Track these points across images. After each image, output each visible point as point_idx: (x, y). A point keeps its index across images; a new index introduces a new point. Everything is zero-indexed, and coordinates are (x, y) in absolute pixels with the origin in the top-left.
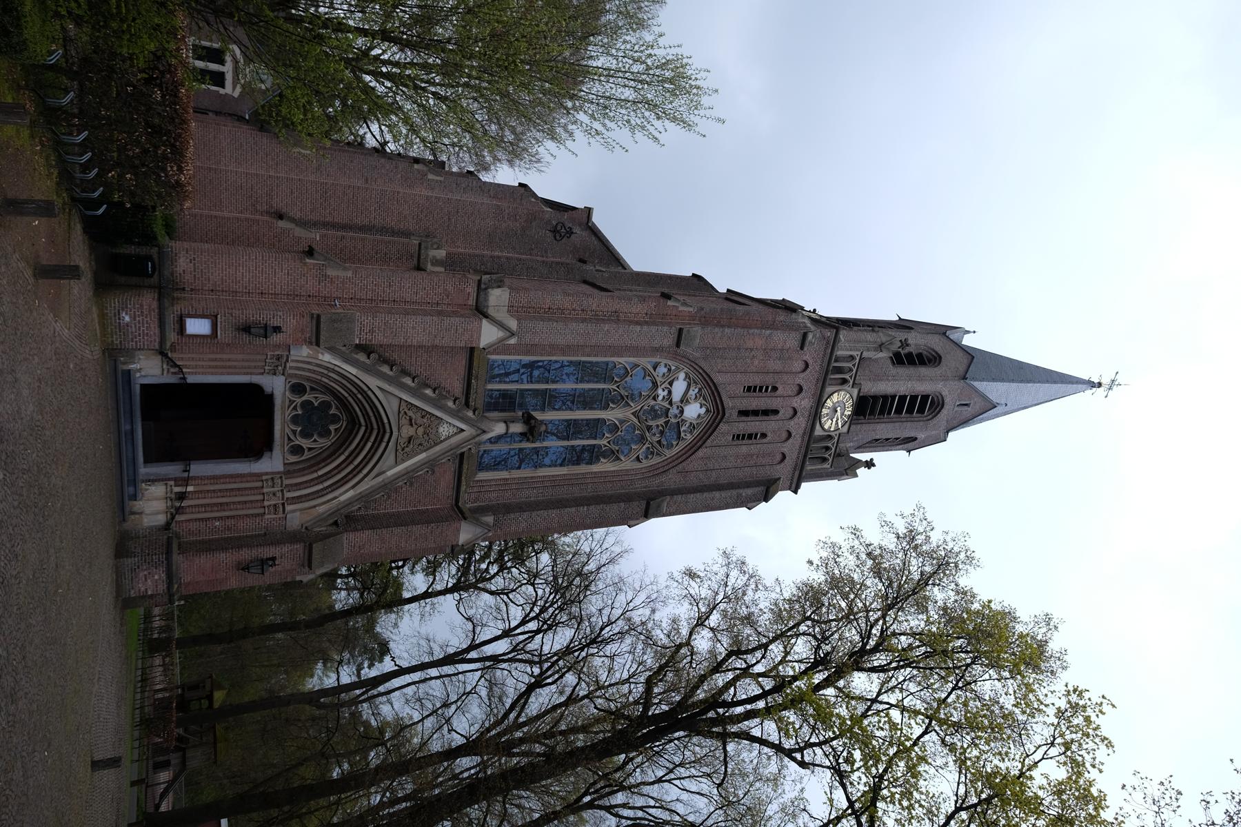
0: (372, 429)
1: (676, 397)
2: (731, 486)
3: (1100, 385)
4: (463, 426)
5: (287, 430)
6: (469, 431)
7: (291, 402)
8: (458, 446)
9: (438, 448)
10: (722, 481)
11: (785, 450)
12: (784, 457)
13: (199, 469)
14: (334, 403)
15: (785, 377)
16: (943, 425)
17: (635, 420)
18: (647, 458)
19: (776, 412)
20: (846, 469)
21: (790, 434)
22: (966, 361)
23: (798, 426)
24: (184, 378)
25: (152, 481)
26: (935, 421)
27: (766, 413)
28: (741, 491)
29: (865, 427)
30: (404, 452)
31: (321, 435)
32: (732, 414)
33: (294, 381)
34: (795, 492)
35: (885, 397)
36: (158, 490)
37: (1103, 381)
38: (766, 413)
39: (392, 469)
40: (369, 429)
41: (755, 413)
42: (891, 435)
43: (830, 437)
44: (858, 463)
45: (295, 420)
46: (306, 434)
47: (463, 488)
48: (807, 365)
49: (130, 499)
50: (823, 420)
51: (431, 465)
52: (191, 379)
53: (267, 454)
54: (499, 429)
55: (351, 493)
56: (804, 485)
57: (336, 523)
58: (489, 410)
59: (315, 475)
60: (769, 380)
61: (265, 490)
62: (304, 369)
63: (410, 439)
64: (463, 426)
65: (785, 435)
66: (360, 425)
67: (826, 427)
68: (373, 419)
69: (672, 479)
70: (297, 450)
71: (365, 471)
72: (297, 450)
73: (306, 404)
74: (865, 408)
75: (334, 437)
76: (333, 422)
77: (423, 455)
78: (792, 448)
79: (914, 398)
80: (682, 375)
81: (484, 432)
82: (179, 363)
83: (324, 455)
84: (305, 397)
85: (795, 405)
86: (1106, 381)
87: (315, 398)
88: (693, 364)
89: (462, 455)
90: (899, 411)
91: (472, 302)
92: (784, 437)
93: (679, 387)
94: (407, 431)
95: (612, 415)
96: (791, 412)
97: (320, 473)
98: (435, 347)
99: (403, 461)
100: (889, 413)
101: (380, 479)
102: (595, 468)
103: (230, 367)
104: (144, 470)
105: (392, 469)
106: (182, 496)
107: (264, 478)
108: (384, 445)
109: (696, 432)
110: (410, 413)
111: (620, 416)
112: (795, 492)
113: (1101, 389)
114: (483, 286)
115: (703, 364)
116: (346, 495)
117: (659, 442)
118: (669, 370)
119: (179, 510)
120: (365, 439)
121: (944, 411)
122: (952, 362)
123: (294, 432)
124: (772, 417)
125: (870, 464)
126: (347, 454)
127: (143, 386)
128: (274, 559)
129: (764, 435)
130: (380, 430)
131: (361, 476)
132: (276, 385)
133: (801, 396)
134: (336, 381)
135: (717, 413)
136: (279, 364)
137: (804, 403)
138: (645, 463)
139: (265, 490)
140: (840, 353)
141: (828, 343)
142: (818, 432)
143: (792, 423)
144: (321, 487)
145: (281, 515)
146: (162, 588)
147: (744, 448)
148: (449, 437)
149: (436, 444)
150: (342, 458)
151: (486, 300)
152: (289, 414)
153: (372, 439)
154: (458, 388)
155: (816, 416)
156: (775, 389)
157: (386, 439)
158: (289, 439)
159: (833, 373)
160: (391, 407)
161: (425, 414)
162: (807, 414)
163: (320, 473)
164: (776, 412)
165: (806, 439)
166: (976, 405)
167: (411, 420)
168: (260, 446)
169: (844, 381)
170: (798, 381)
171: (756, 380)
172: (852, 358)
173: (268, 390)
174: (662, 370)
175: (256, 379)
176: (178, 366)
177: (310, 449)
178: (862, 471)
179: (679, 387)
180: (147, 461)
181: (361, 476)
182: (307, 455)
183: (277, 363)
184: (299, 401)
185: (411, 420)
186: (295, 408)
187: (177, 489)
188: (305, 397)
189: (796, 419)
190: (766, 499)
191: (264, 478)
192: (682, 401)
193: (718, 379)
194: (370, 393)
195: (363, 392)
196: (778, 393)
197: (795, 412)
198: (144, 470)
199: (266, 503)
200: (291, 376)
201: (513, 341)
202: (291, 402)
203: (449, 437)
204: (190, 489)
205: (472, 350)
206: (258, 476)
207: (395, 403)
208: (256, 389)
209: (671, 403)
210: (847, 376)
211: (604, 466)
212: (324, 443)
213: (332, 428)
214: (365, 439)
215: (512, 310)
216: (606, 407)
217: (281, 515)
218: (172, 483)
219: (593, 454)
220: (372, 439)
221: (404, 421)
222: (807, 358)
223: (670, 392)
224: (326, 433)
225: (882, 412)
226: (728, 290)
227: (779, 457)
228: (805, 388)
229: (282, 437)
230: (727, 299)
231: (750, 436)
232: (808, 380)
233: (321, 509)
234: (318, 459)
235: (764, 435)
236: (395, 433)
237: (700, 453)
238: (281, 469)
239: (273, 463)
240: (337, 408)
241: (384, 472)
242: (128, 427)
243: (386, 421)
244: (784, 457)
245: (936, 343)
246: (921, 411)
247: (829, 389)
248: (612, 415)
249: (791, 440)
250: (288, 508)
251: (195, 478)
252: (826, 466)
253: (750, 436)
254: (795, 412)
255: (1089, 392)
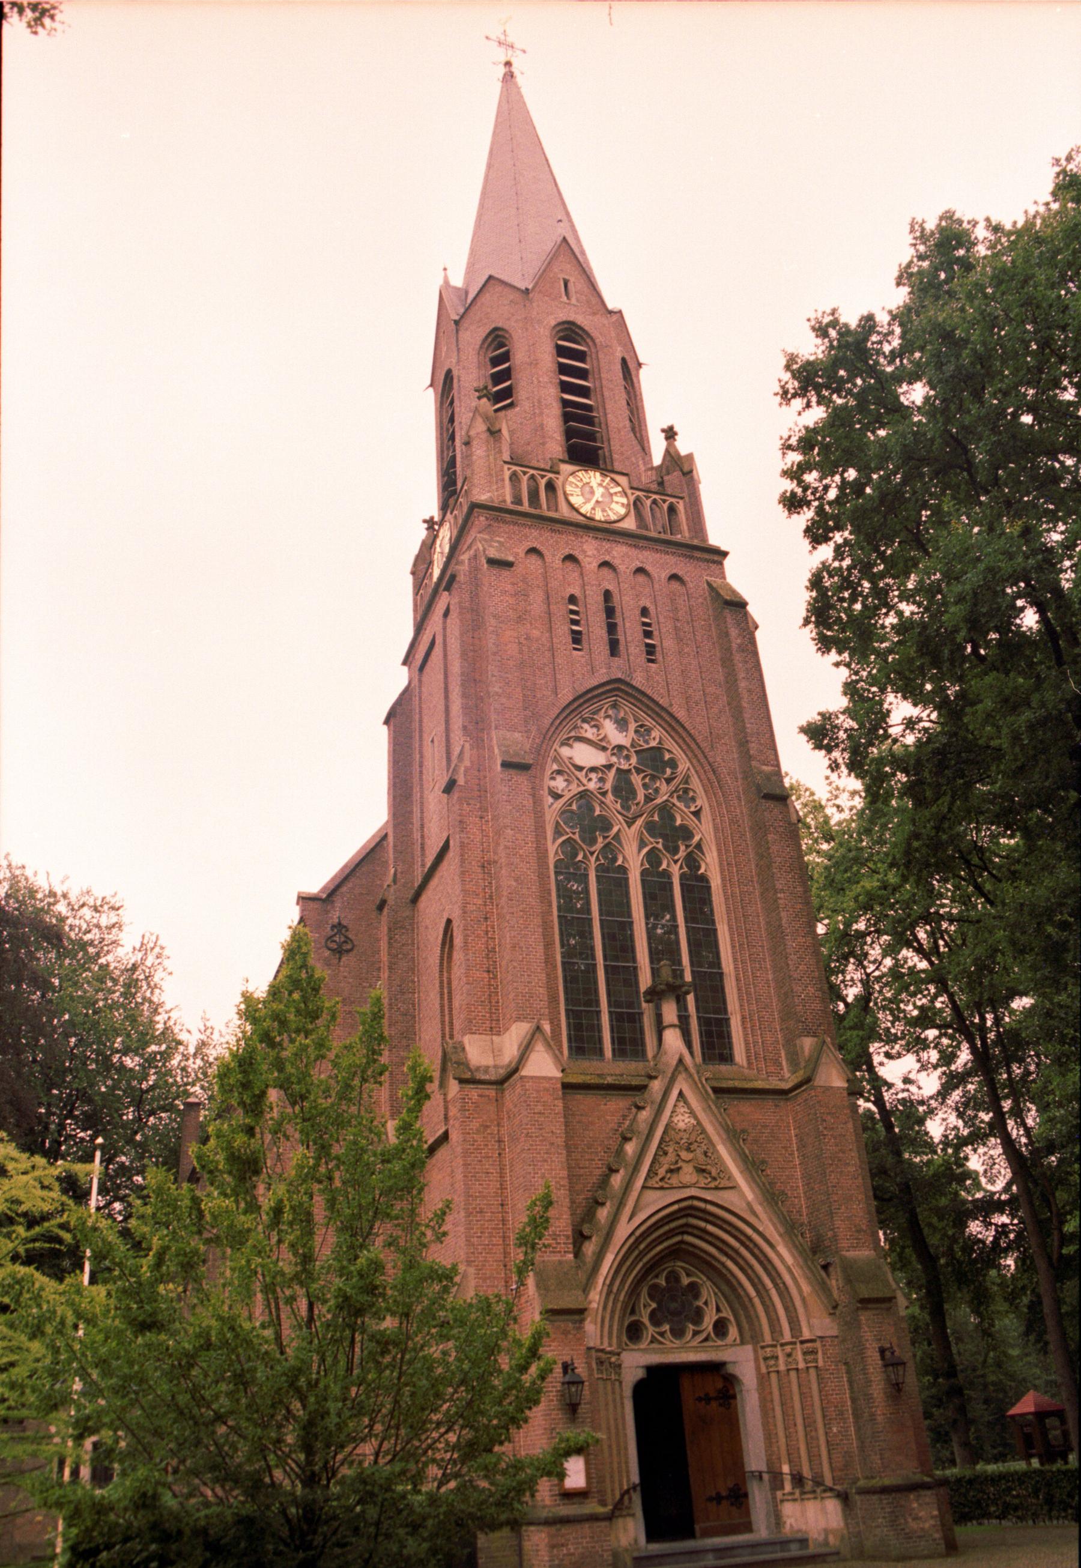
0: (687, 1225)
1: (598, 759)
2: (727, 661)
3: (508, 64)
4: (675, 1093)
5: (694, 1343)
6: (682, 1084)
7: (653, 1340)
8: (704, 1097)
9: (709, 1129)
10: (720, 677)
11: (664, 575)
12: (674, 577)
13: (755, 1458)
14: (651, 1281)
15: (554, 584)
16: (602, 320)
17: (640, 822)
18: (693, 799)
19: (607, 595)
20: (680, 468)
21: (640, 570)
22: (499, 288)
23: (621, 554)
24: (634, 1488)
25: (778, 1520)
26: (594, 333)
27: (610, 612)
28: (734, 646)
29: (615, 445)
30: (718, 1179)
31: (697, 1296)
32: (617, 669)
33: (625, 1338)
34: (725, 554)
35: (567, 417)
36: (789, 1510)
37: (503, 59)
38: (610, 612)
39: (742, 1194)
40: (685, 1229)
41: (612, 628)
42: (621, 397)
43: (637, 504)
44: (671, 455)
45: (678, 1333)
46: (698, 1316)
47: (759, 1084)
48: (533, 551)
49: (807, 1547)
50: (613, 517)
51: (734, 1135)
52: (635, 1478)
53: (731, 1369)
54: (673, 1039)
55: (782, 1250)
56: (715, 539)
57: (825, 1267)
58: (644, 1053)
59: (757, 1301)
60: (560, 610)
61: (782, 1367)
62: (611, 1327)
63: (701, 1171)
64: (675, 1093)
65: (641, 578)
66: (682, 1242)
67: (622, 511)
68: (673, 1225)
69: (726, 757)
70: (720, 1328)
71: (749, 1231)
72: (720, 1328)
73: (655, 1319)
74: (585, 449)
75: (700, 1279)
76: (677, 1279)
77: (723, 1150)
78: (660, 564)
79: (563, 369)
80: (565, 752)
81: (681, 1061)
82: (618, 1497)
83: (724, 1287)
84: (646, 1320)
85: (595, 564)
86: (502, 56)
87: (646, 1308)
88: (547, 737)
89: (716, 1090)
90: (584, 392)
91: (491, 1092)
92: (641, 581)
93: (585, 755)
94: (688, 1174)
95: (633, 859)
96: (605, 571)
97: (752, 1292)
98: (567, 1147)
99: (730, 1177)
100: (588, 408)
101: (758, 1209)
102: (716, 882)
103: (617, 1428)
104: (762, 1531)
105: (742, 1194)
106: (798, 1480)
107: (764, 1370)
108: (710, 1208)
109: (649, 722)
110: (662, 1172)
111: (635, 846)
112: (725, 554)
113: (513, 60)
114: (468, 1076)
115: (547, 721)
116: (784, 1256)
117: (668, 781)
118: (559, 772)
119: (818, 1482)
120: (703, 1235)
121: (580, 320)
122: (498, 312)
123: (696, 1333)
124: (616, 598)
125: (670, 434)
126: (724, 1259)
127: (651, 1537)
128: (882, 1351)
129: (645, 612)
130: (687, 1216)
131: (755, 1237)
132: (635, 1362)
133: (580, 557)
134: (623, 1282)
135: (617, 691)
136: (606, 1362)
137: (590, 551)
138: (702, 801)
139: (782, 1367)
140: (509, 499)
141: (497, 520)
142: (630, 524)
143: (622, 568)
144: (774, 1293)
145: (818, 1344)
146: (928, 1496)
147: (666, 641)
148: (692, 1113)
149: (703, 1131)
150: (730, 1264)
151: (487, 1069)
152: (670, 1342)
153: (702, 1224)
154: (615, 1106)
155: (607, 531)
156: (572, 599)
157: (702, 1205)
158: (706, 1339)
159: (536, 509)
160: (656, 1202)
161: (661, 1151)
162: (607, 545)
163: (752, 1292)
164: (607, 595)
165: (642, 543)
166: (565, 269)
167: (671, 1171)
168: (719, 1380)
169: (551, 487)
170: (557, 563)
171: (563, 630)
172: (514, 478)
173: (640, 1374)
174: (560, 783)
175: (628, 1392)
176: (622, 1496)
177: (718, 1310)
178: (683, 447)
179: (585, 755)
180: (748, 1527)
181: (755, 1237)
182: (727, 1313)
183: (607, 1364)
184: (651, 1330)
185: (671, 1171)
186: (662, 1334)
187: (788, 1487)
188: (646, 1320)
189: (616, 562)
190: (742, 605)
191: (764, 1370)
192: (604, 749)
193: (566, 695)
194: (638, 1233)
195: (639, 1241)
196: (576, 591)
197: (605, 564)
198: (762, 1531)
199: (802, 1365)
200: (619, 1345)
201: (547, 1027)
202: (653, 1340)
203: (692, 1113)
204: (786, 1469)
205: (566, 1086)
206: (763, 1380)
207: (651, 1195)
208: (640, 1390)
209: (609, 767)
210: (543, 483)
211: (711, 865)
212: (708, 1293)
213: (686, 1281)
214: (703, 1235)
215: (495, 1028)
216: (623, 870)
217: (818, 1344)
218: (779, 1494)
219: (697, 890)
220: (702, 1224)
221: (674, 1181)
222: (521, 551)
223: (593, 769)
224: (694, 1290)
225: (590, 421)
226: (405, 662)
227: (675, 585)
228: (567, 552)
229: (705, 1349)
230: (422, 668)
231: (648, 634)
232: (555, 546)
233: (806, 1288)
234: (732, 1297)
235: (645, 612)
236: (693, 1192)
237: (681, 714)
238: (749, 1348)
239: (743, 1361)
240: (657, 1276)
241: (749, 1204)
242: (710, 1556)
243: (676, 1207)
244: (674, 577)
245: (474, 335)
246: (581, 356)
247: (565, 512)
248: (633, 859)
249: (648, 568)
250: (806, 1334)
251: (769, 1463)
252: (681, 507)
253: (648, 634)
254: (605, 564)
255: (520, 79)
